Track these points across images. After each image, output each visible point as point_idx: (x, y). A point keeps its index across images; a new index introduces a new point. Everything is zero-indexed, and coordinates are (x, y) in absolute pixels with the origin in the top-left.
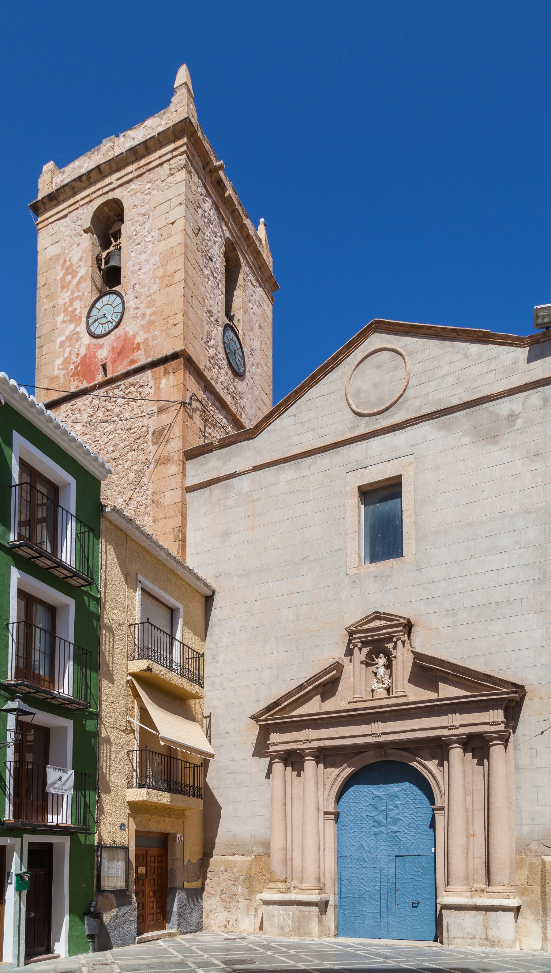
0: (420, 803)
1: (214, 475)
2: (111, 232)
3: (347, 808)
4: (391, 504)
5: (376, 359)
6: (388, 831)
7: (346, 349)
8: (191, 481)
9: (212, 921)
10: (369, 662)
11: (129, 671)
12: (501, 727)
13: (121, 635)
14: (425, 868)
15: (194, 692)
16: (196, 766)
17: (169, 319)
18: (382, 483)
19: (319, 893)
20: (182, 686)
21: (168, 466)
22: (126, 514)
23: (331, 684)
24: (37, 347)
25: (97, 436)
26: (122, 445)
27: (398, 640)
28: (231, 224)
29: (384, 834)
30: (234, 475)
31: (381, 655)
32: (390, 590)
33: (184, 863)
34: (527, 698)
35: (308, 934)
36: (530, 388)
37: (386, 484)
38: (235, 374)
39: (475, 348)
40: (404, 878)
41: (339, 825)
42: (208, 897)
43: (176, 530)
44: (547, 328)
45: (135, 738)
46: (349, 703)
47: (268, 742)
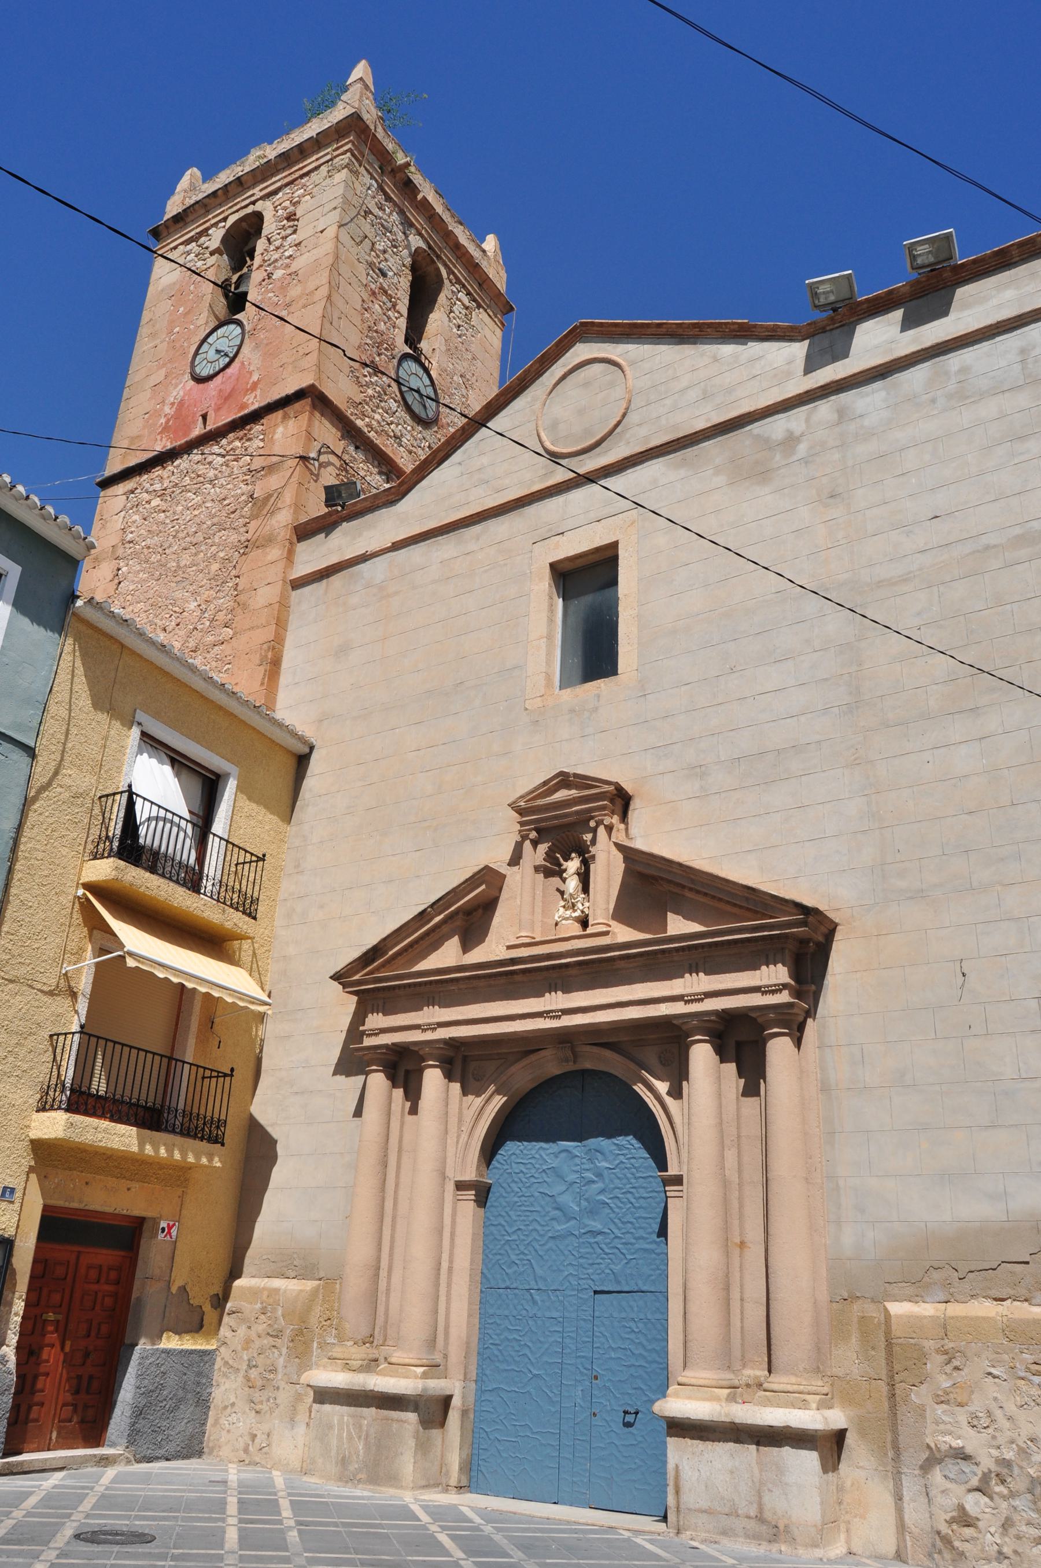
0: (645, 1167)
1: (334, 560)
2: (246, 249)
3: (506, 1175)
4: (607, 592)
5: (583, 375)
6: (583, 1231)
7: (538, 365)
8: (301, 569)
9: (224, 1433)
10: (552, 870)
11: (84, 879)
12: (784, 997)
13: (78, 813)
14: (652, 1323)
15: (229, 925)
16: (214, 1074)
17: (299, 349)
18: (590, 557)
19: (425, 1376)
20: (199, 913)
21: (268, 550)
22: (116, 611)
23: (480, 911)
24: (124, 398)
25: (178, 512)
26: (209, 523)
27: (599, 823)
28: (426, 230)
29: (573, 1238)
30: (364, 558)
31: (573, 855)
32: (594, 734)
33: (169, 1288)
34: (838, 936)
35: (393, 1479)
36: (815, 396)
37: (597, 557)
38: (417, 420)
39: (727, 350)
40: (610, 1347)
41: (488, 1214)
42: (225, 1375)
43: (265, 646)
44: (835, 310)
45: (76, 1012)
46: (509, 947)
47: (361, 1028)
